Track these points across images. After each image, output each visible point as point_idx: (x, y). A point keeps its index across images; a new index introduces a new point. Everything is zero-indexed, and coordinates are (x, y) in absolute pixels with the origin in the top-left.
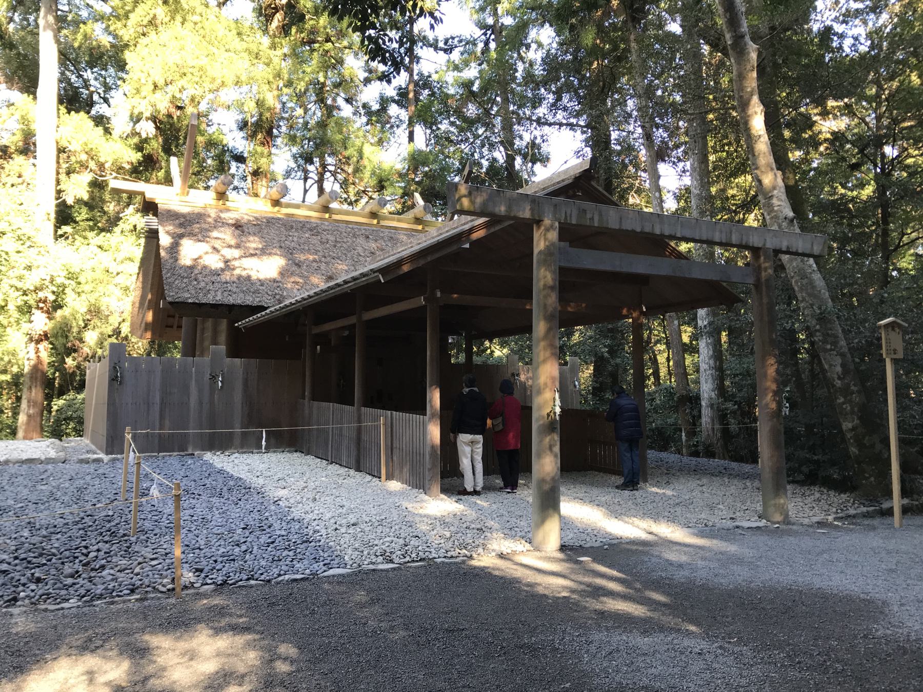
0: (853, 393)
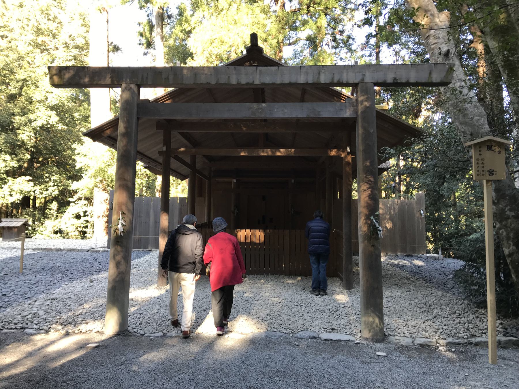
0: (508, 218)
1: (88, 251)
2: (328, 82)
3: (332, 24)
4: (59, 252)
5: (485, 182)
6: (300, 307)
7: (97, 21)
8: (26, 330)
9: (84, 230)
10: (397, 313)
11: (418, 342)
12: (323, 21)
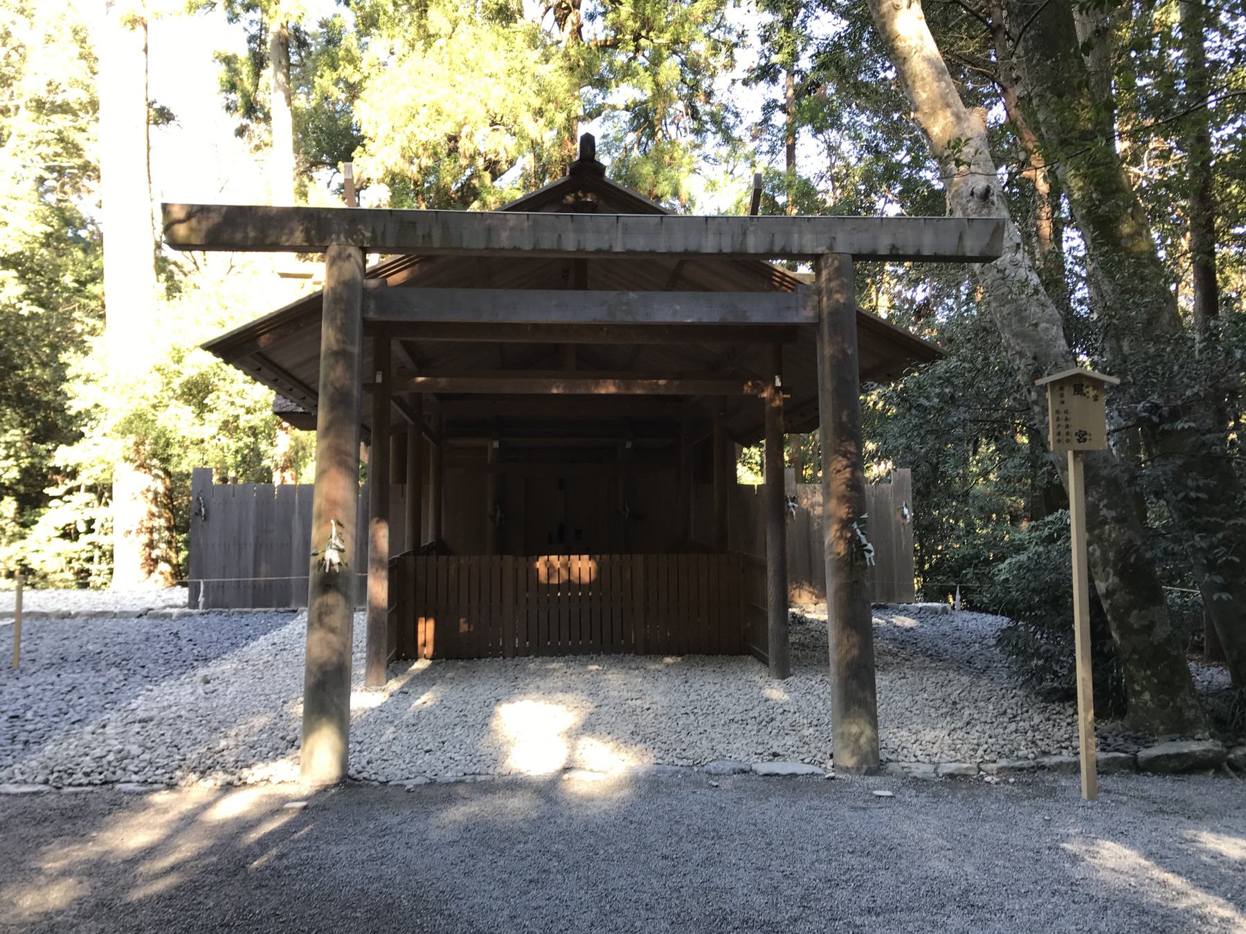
0: (1104, 522)
1: (141, 616)
2: (761, 251)
3: (689, 77)
4: (67, 621)
5: (1070, 454)
6: (692, 717)
7: (112, 42)
8: (118, 786)
9: (87, 566)
10: (892, 720)
11: (945, 771)
12: (670, 69)
